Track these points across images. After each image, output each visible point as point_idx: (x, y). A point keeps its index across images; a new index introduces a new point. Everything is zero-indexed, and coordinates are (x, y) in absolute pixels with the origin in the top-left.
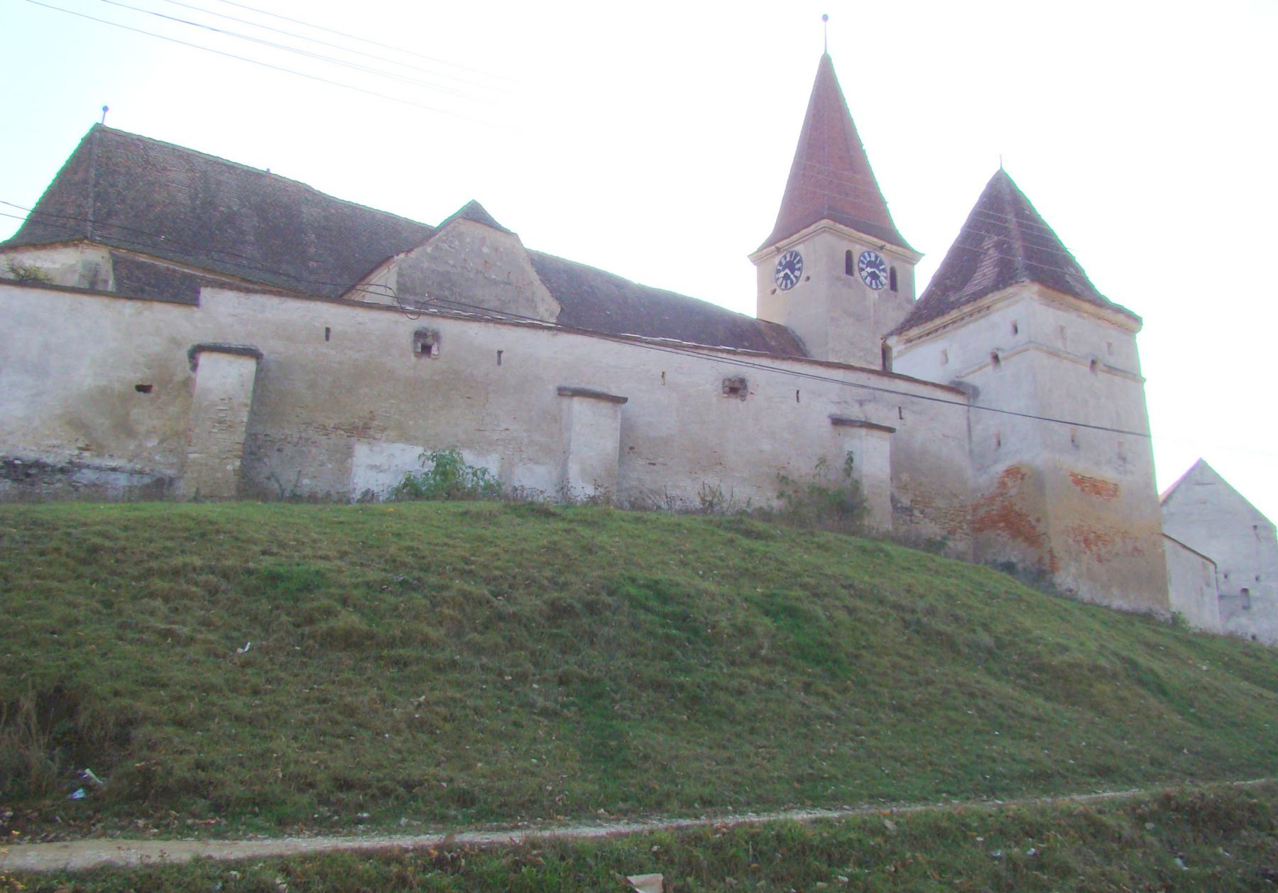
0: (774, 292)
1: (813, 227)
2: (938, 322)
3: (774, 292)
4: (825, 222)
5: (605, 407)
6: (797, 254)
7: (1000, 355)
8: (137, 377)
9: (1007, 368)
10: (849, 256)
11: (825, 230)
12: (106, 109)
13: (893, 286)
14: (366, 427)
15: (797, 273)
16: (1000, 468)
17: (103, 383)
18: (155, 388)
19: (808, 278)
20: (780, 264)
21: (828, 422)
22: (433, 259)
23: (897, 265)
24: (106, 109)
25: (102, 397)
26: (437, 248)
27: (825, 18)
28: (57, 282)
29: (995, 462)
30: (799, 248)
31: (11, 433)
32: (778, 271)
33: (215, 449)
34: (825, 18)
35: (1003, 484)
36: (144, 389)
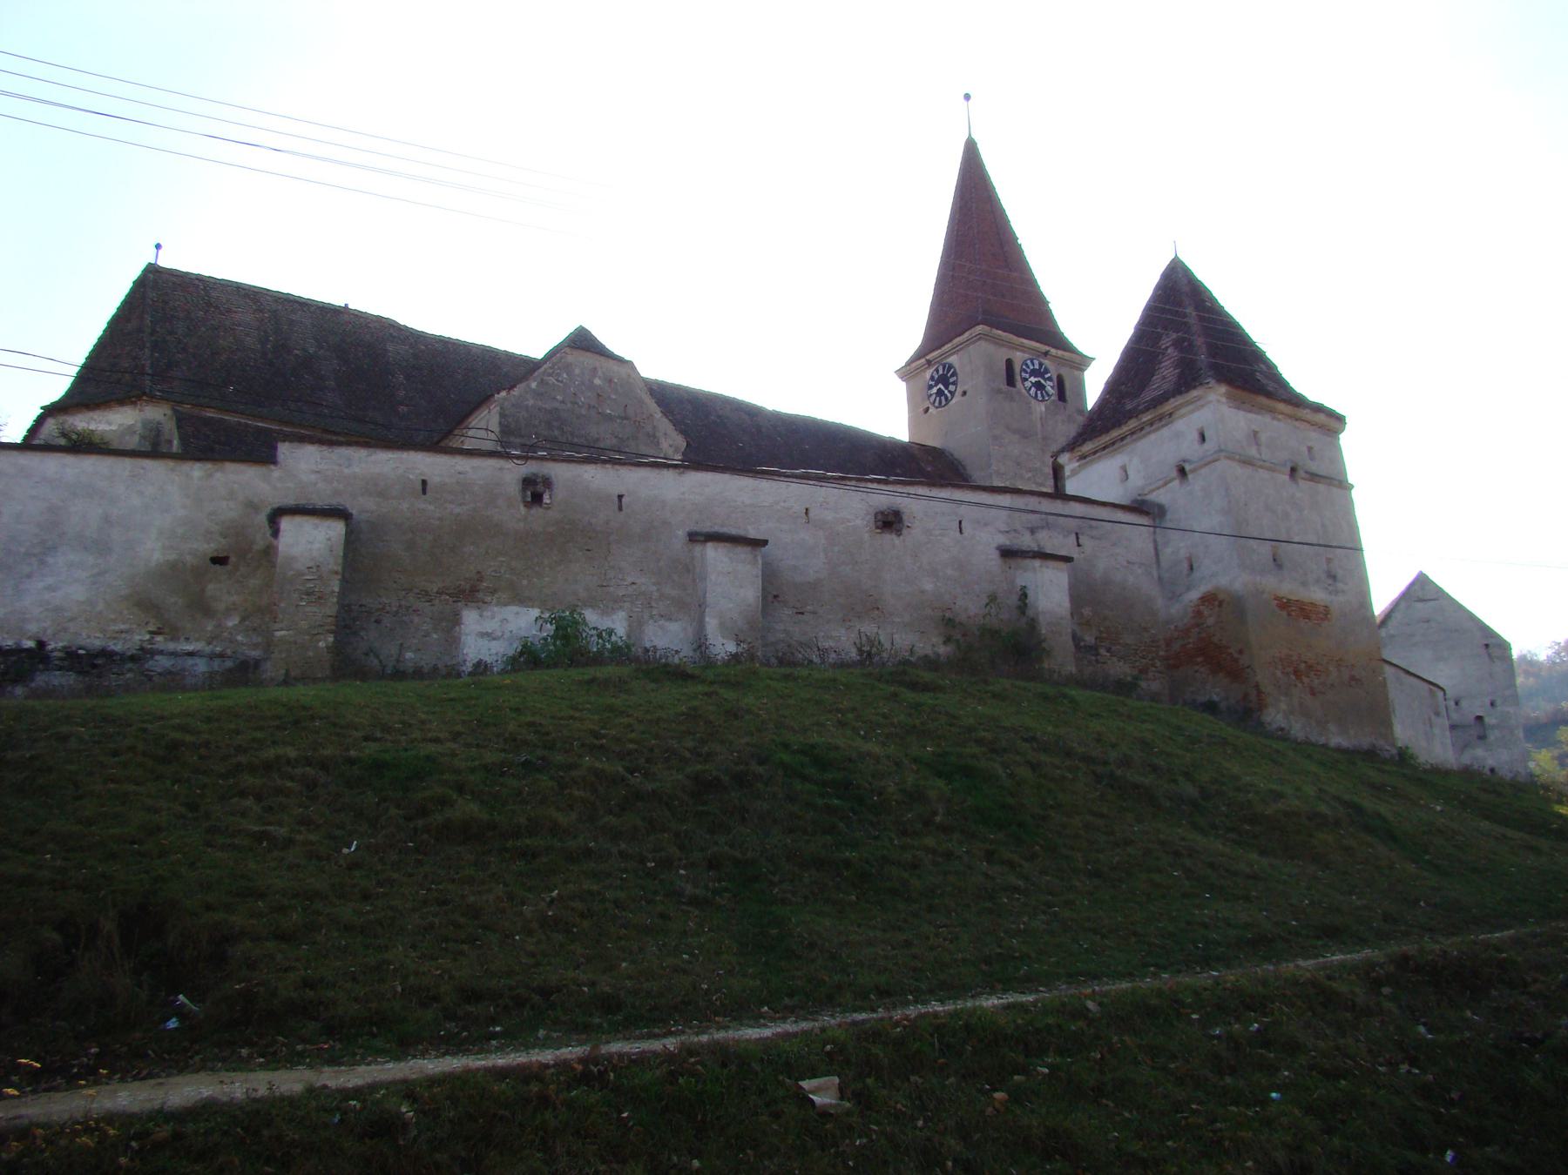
0: (927, 410)
1: (966, 335)
2: (1115, 434)
3: (927, 410)
4: (979, 328)
5: (743, 552)
6: (951, 366)
7: (1187, 467)
8: (209, 548)
9: (1196, 482)
10: (1009, 363)
11: (980, 337)
12: (158, 247)
13: (1062, 395)
14: (474, 590)
15: (952, 388)
16: (1194, 595)
17: (172, 557)
18: (233, 559)
19: (964, 393)
20: (932, 378)
21: (995, 555)
22: (538, 394)
23: (1064, 372)
24: (158, 247)
25: (172, 573)
26: (542, 382)
27: (967, 97)
28: (115, 445)
29: (1189, 589)
30: (953, 359)
31: (72, 619)
32: (930, 387)
33: (304, 624)
34: (967, 97)
35: (1198, 613)
36: (219, 561)
